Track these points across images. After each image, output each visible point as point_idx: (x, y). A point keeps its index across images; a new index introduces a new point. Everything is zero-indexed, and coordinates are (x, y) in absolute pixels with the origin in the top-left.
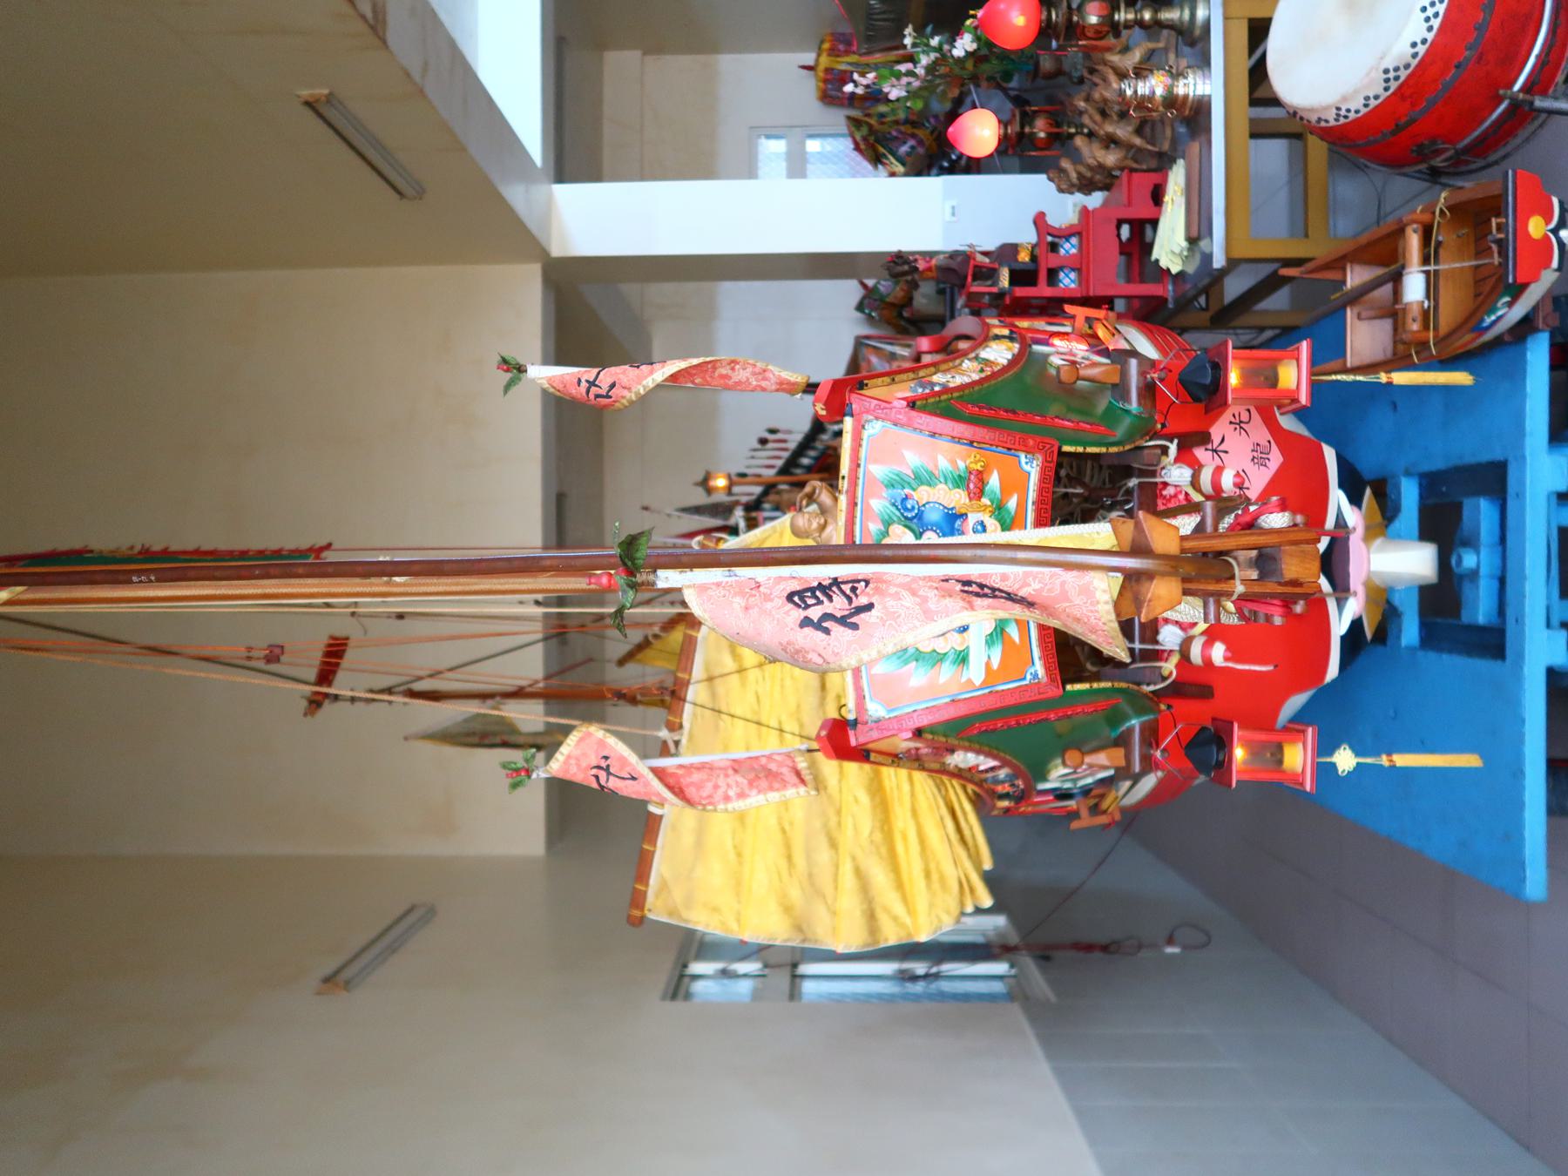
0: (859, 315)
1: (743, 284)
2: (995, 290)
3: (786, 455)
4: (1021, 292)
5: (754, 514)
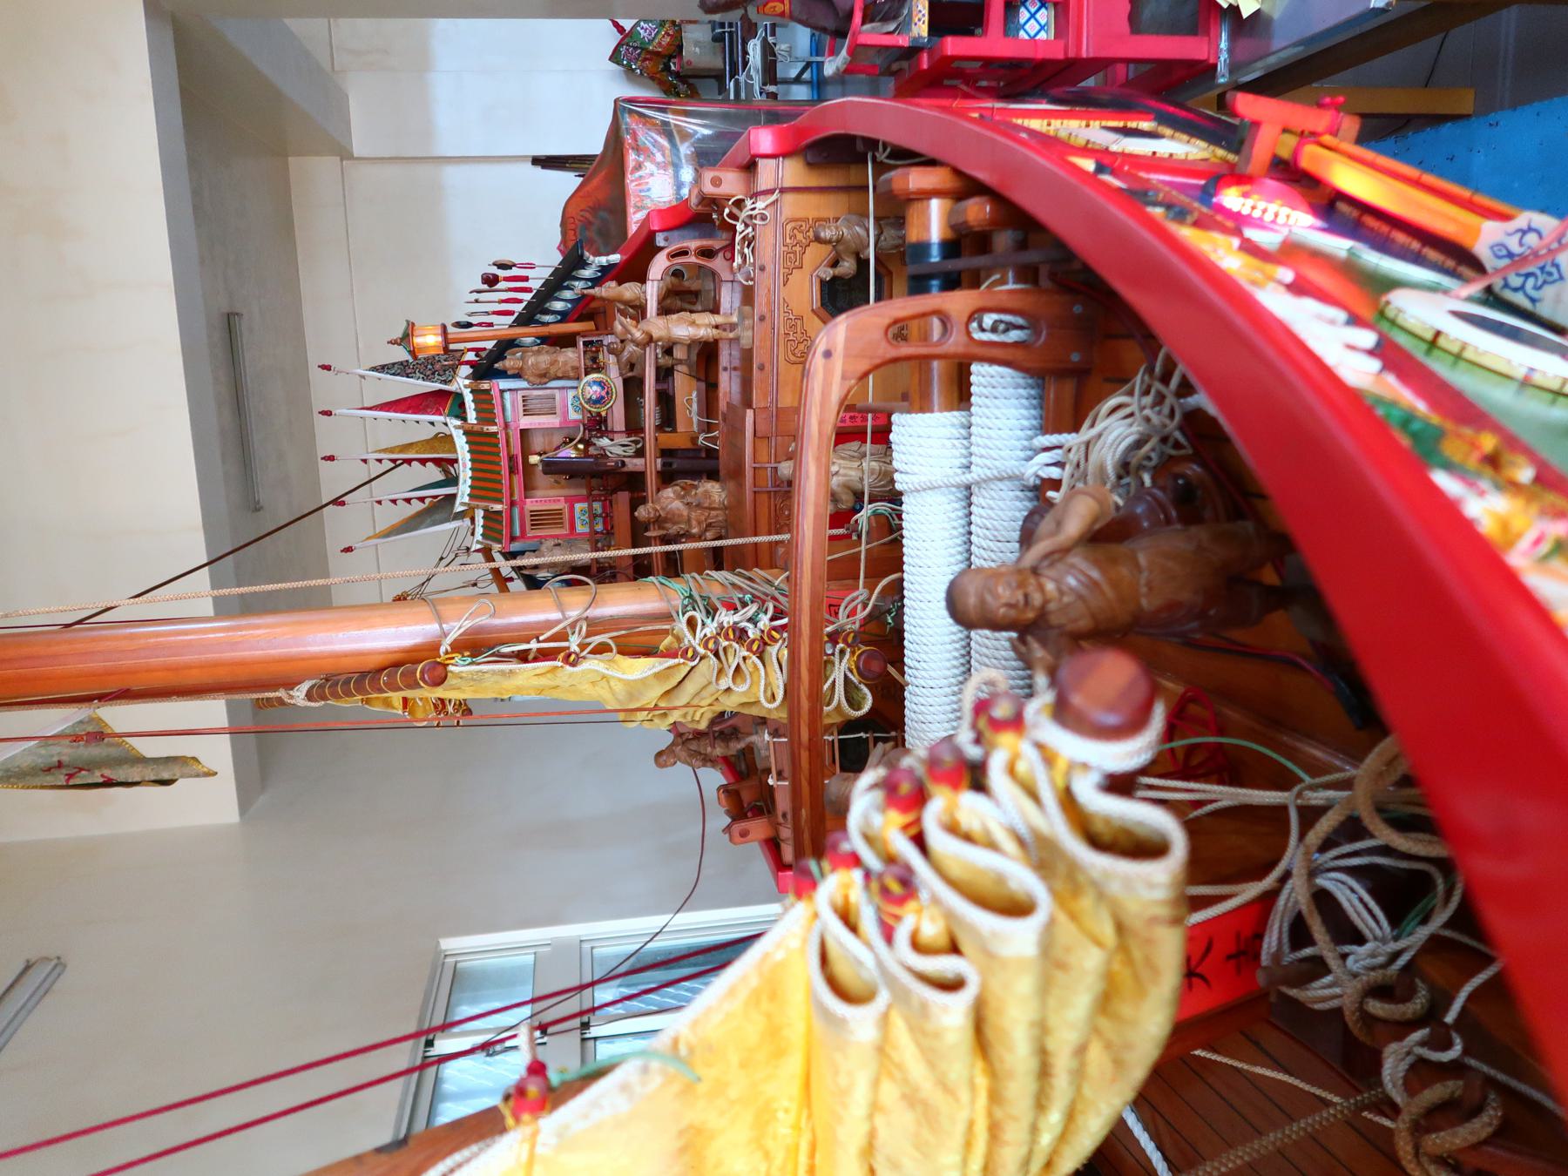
1: (464, 23)
2: (903, 41)
3: (527, 297)
4: (953, 45)
5: (485, 385)
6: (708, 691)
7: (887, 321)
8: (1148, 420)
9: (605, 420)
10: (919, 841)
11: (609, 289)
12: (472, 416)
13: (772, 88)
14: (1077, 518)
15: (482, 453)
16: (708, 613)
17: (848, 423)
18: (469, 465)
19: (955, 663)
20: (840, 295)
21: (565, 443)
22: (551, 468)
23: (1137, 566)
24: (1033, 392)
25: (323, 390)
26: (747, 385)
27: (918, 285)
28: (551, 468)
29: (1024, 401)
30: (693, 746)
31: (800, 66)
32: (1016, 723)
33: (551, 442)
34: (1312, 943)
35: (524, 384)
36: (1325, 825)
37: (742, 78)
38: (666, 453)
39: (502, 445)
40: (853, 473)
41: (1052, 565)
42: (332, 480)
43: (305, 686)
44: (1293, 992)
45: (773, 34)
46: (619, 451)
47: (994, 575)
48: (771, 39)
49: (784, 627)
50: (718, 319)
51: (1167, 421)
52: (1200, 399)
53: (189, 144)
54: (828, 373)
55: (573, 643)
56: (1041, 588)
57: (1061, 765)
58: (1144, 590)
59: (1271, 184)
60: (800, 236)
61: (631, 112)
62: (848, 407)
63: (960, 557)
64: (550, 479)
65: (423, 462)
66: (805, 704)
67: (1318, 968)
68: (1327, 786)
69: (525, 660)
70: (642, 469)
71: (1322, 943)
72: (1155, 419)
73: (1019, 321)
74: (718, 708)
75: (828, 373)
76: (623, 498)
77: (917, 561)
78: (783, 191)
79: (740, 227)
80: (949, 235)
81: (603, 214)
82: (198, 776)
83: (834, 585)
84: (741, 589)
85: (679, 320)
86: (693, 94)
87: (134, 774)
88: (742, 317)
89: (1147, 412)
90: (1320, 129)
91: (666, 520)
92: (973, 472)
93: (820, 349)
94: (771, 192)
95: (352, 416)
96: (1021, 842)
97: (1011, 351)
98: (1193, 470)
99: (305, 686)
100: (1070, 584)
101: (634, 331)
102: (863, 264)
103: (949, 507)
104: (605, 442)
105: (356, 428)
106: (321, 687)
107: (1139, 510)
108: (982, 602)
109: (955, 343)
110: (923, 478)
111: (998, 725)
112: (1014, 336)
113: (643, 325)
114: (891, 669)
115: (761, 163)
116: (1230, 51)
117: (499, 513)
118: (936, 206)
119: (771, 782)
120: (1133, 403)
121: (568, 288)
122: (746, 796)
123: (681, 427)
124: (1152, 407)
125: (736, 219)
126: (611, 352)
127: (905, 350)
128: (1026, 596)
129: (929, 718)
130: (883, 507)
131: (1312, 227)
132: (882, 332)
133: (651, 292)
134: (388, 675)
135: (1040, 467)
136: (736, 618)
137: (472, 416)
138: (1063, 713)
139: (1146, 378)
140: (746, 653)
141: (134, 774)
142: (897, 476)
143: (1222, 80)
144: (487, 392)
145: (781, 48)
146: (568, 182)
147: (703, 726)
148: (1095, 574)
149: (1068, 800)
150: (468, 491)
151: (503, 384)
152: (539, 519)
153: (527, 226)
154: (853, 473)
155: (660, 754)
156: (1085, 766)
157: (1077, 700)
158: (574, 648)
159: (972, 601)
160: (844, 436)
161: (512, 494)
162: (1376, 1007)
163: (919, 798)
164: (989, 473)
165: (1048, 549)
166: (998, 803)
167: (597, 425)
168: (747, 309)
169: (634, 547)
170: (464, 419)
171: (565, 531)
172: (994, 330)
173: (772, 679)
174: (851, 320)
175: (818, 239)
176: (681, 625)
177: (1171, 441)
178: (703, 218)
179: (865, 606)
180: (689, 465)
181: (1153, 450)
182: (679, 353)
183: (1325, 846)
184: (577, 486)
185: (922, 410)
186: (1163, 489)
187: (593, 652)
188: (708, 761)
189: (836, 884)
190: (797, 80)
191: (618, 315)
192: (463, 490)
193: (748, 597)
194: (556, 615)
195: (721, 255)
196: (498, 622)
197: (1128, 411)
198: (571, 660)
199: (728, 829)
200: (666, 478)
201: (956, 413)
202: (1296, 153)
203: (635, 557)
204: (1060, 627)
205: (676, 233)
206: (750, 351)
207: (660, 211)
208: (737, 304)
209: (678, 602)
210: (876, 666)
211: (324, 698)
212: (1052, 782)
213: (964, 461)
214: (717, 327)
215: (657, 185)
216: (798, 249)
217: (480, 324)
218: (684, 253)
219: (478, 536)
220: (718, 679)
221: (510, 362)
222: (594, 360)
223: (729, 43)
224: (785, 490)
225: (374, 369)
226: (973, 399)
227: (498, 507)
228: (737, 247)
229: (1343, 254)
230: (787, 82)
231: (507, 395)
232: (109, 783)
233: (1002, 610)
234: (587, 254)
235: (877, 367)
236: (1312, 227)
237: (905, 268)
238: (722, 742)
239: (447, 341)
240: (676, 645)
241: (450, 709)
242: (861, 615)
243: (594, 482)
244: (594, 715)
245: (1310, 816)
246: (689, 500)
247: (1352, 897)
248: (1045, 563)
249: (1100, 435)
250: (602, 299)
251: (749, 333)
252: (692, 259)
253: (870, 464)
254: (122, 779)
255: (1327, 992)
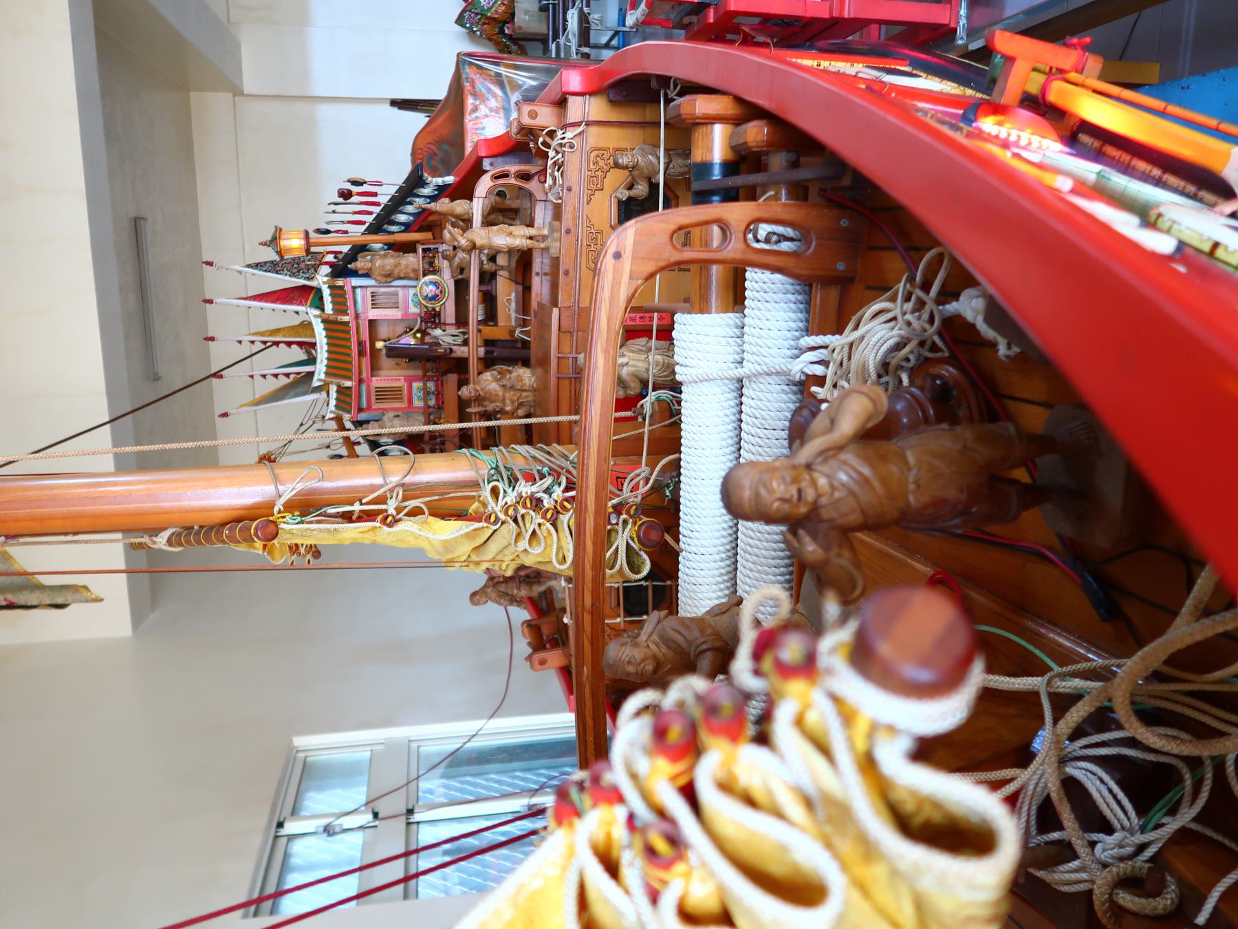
0: (459, 28)
3: (377, 210)
5: (340, 282)
6: (509, 550)
7: (673, 227)
8: (909, 324)
9: (438, 315)
10: (689, 793)
11: (443, 205)
12: (329, 308)
13: (586, 50)
14: (853, 414)
15: (337, 338)
16: (510, 482)
17: (638, 322)
18: (326, 348)
19: (724, 533)
20: (629, 209)
21: (406, 332)
22: (393, 352)
23: (906, 462)
24: (800, 297)
25: (212, 281)
26: (554, 287)
27: (702, 197)
28: (393, 352)
29: (792, 305)
30: (502, 588)
31: (610, 33)
32: (808, 667)
33: (394, 332)
34: (1060, 827)
35: (372, 282)
36: (1076, 715)
37: (562, 40)
38: (488, 343)
39: (353, 332)
40: (640, 364)
41: (825, 461)
42: (220, 355)
43: (165, 535)
44: (1040, 874)
45: (588, 5)
46: (450, 340)
47: (769, 469)
48: (586, 10)
49: (573, 498)
50: (532, 231)
51: (927, 326)
52: (969, 306)
53: (102, 78)
54: (617, 273)
55: (391, 507)
56: (814, 483)
57: (862, 726)
58: (912, 487)
59: (1025, 114)
60: (602, 163)
61: (470, 64)
62: (633, 308)
63: (730, 442)
64: (391, 362)
65: (289, 344)
66: (589, 573)
67: (1065, 852)
68: (1075, 675)
69: (351, 521)
70: (466, 355)
71: (1071, 830)
72: (915, 324)
73: (789, 232)
74: (519, 562)
75: (617, 273)
76: (452, 378)
77: (693, 443)
78: (588, 124)
79: (551, 153)
80: (730, 156)
81: (446, 147)
82: (87, 601)
83: (620, 460)
84: (541, 462)
85: (498, 231)
86: (523, 52)
87: (32, 598)
88: (552, 230)
89: (908, 317)
90: (1067, 67)
91: (484, 399)
92: (747, 371)
93: (611, 250)
94: (578, 124)
95: (230, 305)
96: (809, 803)
97: (783, 258)
98: (949, 371)
99: (165, 535)
100: (841, 479)
101: (460, 238)
102: (654, 187)
103: (722, 398)
104: (438, 332)
105: (237, 315)
106: (179, 535)
107: (899, 407)
108: (757, 495)
109: (734, 250)
110: (700, 371)
111: (786, 671)
112: (785, 246)
113: (468, 234)
114: (668, 538)
115: (571, 99)
116: (968, 17)
117: (349, 388)
118: (719, 131)
119: (566, 620)
120: (896, 309)
121: (411, 203)
122: (546, 630)
123: (501, 322)
124: (913, 312)
125: (548, 146)
126: (445, 257)
127: (688, 255)
128: (800, 491)
129: (700, 581)
130: (665, 394)
131: (1061, 152)
132: (668, 236)
133: (477, 207)
134: (230, 529)
135: (805, 365)
136: (534, 489)
137: (329, 308)
138: (863, 656)
139: (908, 286)
140: (541, 521)
141: (32, 598)
142: (677, 369)
143: (960, 42)
144: (342, 287)
145: (594, 17)
146: (419, 120)
147: (509, 573)
148: (866, 471)
149: (868, 764)
150: (324, 369)
151: (355, 282)
152: (383, 394)
153: (384, 153)
154: (640, 364)
155: (474, 594)
156: (892, 729)
157: (884, 649)
158: (392, 511)
159: (747, 494)
160: (631, 333)
161: (360, 373)
162: (1126, 899)
163: (691, 749)
164: (759, 368)
165: (825, 445)
166: (782, 757)
167: (432, 318)
168: (556, 223)
169: (460, 421)
170: (323, 310)
171: (404, 405)
172: (767, 241)
173: (563, 543)
174: (639, 225)
175: (617, 165)
176: (486, 493)
177: (929, 343)
178: (523, 145)
179: (647, 480)
180: (507, 353)
181: (912, 352)
182: (502, 260)
183: (1076, 735)
184: (415, 368)
185: (702, 311)
186: (921, 388)
187: (409, 514)
188: (514, 600)
189: (601, 821)
190: (607, 46)
191: (449, 226)
192: (320, 369)
193: (546, 470)
194: (378, 480)
195: (536, 178)
196: (328, 485)
197: (890, 315)
198: (390, 521)
199: (529, 658)
200: (488, 363)
201: (731, 315)
202: (1044, 89)
203: (460, 430)
204: (831, 520)
205: (499, 159)
206: (558, 258)
207: (486, 140)
208: (549, 219)
209: (485, 472)
210: (654, 536)
211: (180, 545)
212: (851, 746)
213: (738, 358)
214: (531, 238)
215: (488, 122)
216: (600, 173)
217: (337, 232)
218: (505, 175)
219: (332, 407)
220: (516, 541)
221: (361, 264)
222: (431, 264)
223: (552, 12)
224: (577, 377)
225: (249, 266)
226: (746, 302)
227: (348, 384)
228: (549, 171)
229: (1092, 178)
230: (598, 47)
231: (358, 291)
232: (11, 606)
233: (776, 504)
234: (426, 175)
235: (662, 269)
236: (1061, 152)
237: (691, 185)
238: (524, 585)
239: (308, 245)
240: (482, 510)
241: (302, 550)
242: (643, 490)
243: (429, 365)
244: (416, 562)
245: (1063, 703)
246: (504, 382)
247: (1102, 788)
248: (820, 460)
249: (863, 338)
250: (436, 213)
251: (557, 244)
252: (512, 181)
253: (656, 357)
254: (22, 602)
255: (1074, 876)
